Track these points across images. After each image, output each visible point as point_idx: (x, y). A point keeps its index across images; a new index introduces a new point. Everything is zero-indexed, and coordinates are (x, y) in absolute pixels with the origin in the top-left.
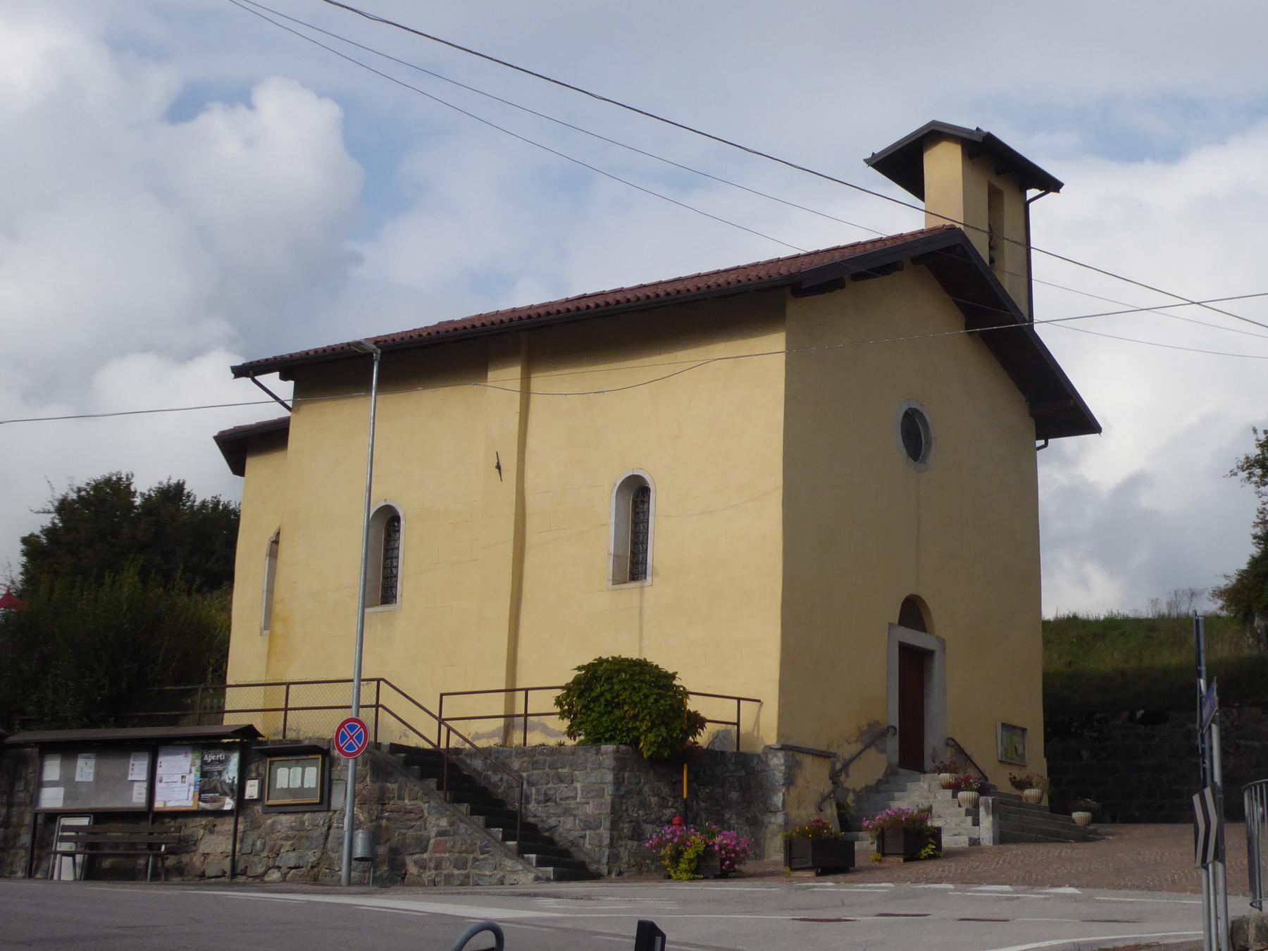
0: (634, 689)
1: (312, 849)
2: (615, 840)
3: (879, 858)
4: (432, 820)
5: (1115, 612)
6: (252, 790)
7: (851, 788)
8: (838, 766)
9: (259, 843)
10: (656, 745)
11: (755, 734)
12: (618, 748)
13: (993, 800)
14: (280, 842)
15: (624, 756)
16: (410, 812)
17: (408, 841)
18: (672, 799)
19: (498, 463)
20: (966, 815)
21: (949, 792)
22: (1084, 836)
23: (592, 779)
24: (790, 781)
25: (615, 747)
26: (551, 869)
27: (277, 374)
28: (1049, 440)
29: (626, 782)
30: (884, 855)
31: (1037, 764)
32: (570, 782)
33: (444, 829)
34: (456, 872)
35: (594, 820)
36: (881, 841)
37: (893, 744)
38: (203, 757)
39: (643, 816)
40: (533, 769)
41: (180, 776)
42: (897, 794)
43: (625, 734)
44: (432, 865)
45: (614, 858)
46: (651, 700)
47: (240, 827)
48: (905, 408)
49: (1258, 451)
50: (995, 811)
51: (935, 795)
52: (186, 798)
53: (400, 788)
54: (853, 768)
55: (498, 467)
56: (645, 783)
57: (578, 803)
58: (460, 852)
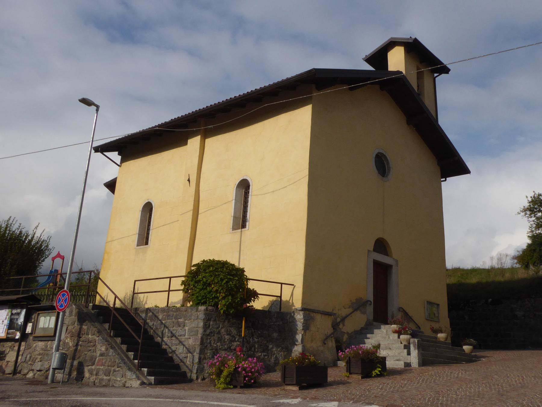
0: (216, 275)
1: (48, 361)
2: (202, 360)
3: (348, 375)
4: (99, 347)
5: (474, 266)
6: (29, 329)
7: (346, 332)
8: (339, 320)
9: (28, 357)
10: (226, 307)
11: (291, 301)
12: (207, 308)
13: (418, 341)
14: (36, 356)
15: (210, 312)
16: (91, 342)
17: (87, 358)
18: (238, 337)
19: (189, 179)
20: (405, 348)
21: (396, 335)
22: (470, 359)
23: (193, 325)
24: (306, 327)
25: (205, 307)
26: (153, 378)
27: (117, 153)
28: (447, 178)
29: (211, 327)
30: (350, 373)
31: (445, 321)
32: (183, 326)
33: (103, 352)
34: (105, 378)
35: (192, 348)
36: (348, 365)
37: (370, 310)
38: (12, 311)
39: (220, 346)
40: (168, 319)
41: (2, 321)
42: (368, 336)
43: (211, 300)
44: (95, 373)
45: (200, 370)
46: (224, 282)
47: (22, 348)
48: (377, 152)
49: (528, 204)
50: (420, 347)
51: (389, 336)
52: (2, 332)
53: (88, 329)
54: (346, 322)
55: (189, 180)
56: (222, 328)
57: (186, 338)
58: (108, 366)
